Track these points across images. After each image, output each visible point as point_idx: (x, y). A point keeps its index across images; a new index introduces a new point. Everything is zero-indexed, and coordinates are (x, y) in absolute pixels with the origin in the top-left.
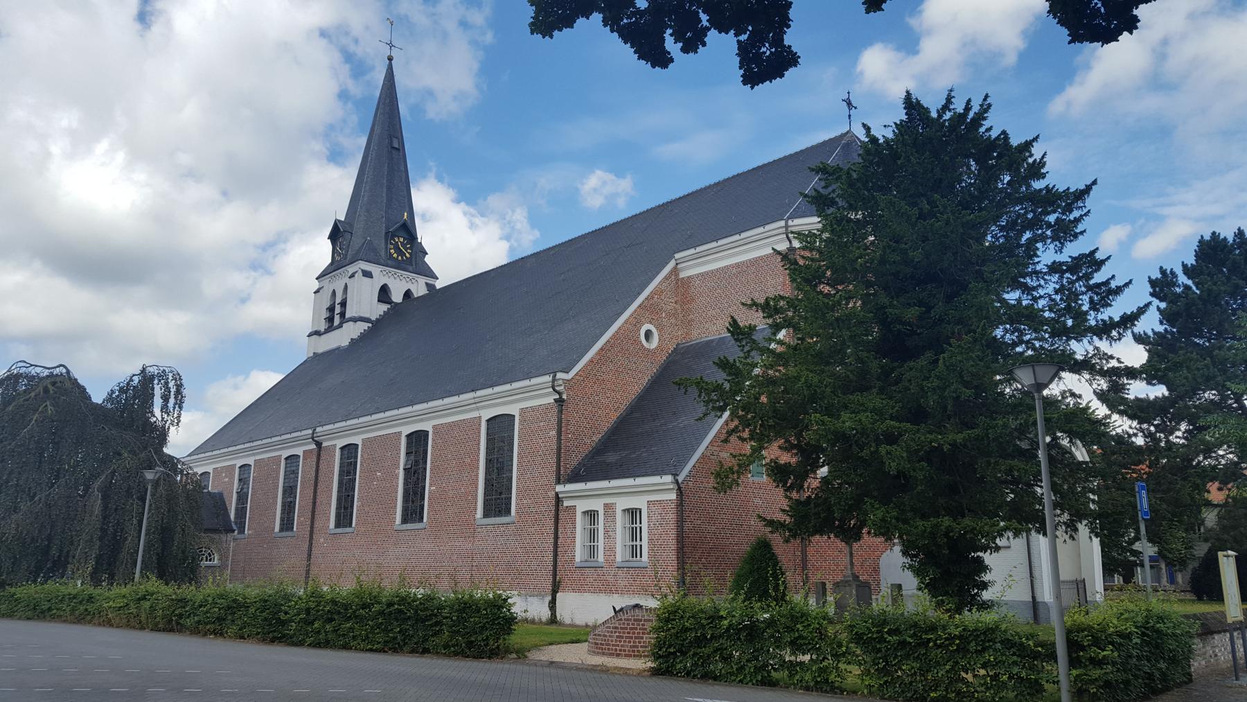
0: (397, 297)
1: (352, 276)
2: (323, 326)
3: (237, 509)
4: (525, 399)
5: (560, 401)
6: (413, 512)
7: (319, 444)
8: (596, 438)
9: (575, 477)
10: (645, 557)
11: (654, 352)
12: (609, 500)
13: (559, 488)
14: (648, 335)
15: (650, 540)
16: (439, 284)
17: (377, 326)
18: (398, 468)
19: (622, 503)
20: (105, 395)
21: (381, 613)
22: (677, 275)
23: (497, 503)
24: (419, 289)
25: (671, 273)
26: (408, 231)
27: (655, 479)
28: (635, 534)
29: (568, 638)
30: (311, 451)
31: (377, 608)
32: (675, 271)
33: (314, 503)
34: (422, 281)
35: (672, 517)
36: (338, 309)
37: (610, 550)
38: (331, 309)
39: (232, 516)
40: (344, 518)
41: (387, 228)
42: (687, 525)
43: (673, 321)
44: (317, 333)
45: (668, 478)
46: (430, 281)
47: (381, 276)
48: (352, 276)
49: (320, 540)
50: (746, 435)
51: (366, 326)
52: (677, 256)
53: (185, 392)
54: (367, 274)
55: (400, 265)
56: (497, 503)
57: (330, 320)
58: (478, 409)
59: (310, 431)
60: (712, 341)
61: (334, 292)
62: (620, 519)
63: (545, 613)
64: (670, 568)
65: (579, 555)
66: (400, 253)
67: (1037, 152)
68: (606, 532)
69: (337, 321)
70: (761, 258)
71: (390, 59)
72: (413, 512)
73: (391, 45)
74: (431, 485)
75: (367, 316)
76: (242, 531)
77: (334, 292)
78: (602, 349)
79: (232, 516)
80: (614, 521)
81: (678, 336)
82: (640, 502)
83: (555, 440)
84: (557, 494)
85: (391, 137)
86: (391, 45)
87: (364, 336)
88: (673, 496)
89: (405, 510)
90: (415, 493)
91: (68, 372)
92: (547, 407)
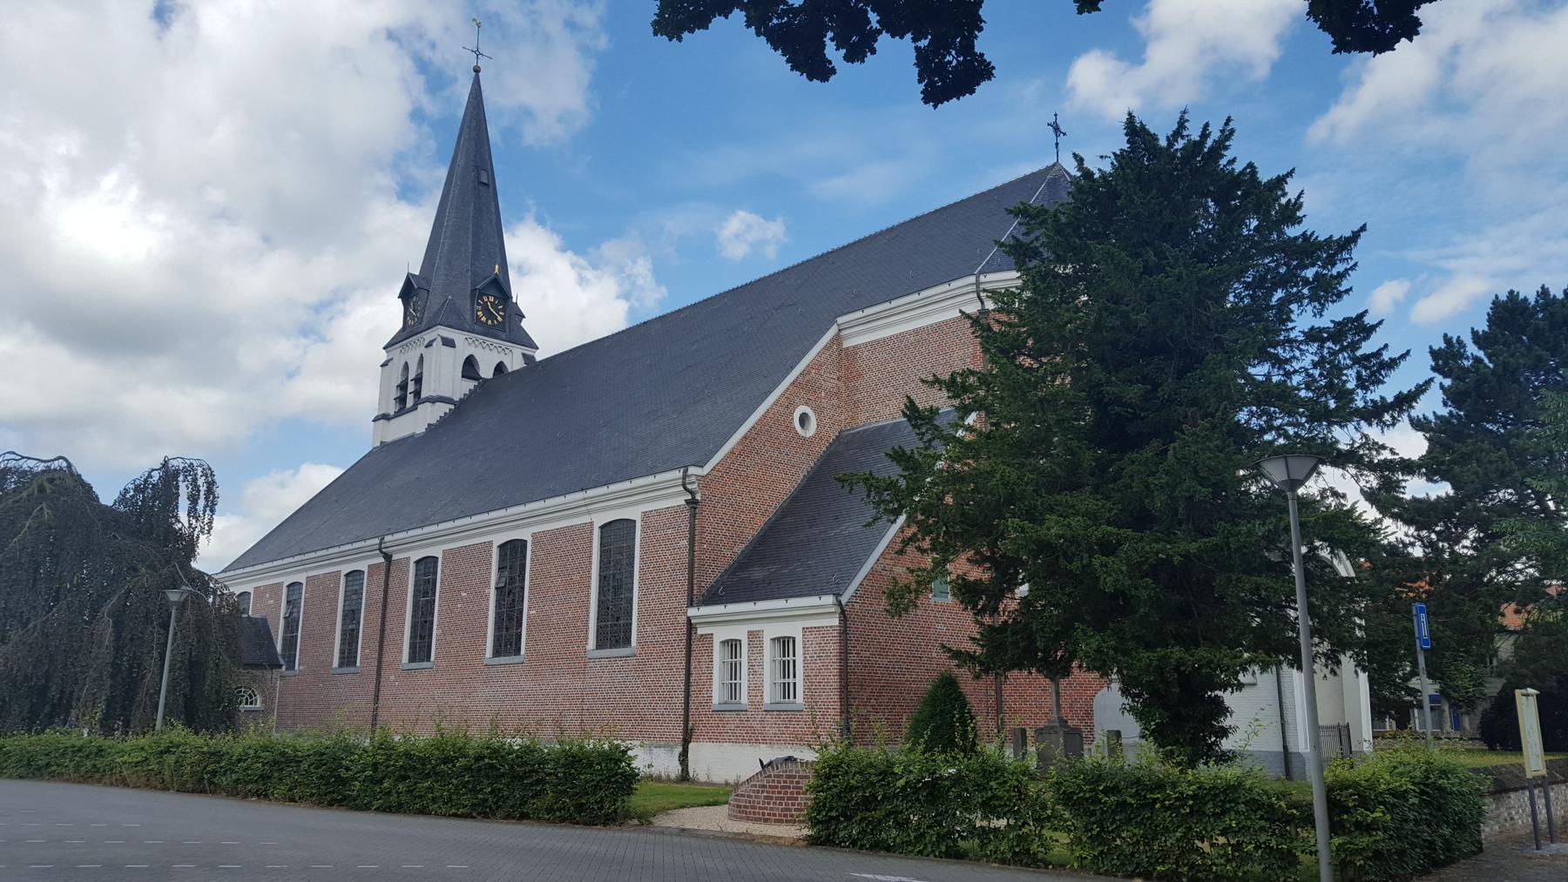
0: (486, 371)
1: (429, 345)
2: (392, 408)
3: (284, 639)
4: (648, 500)
5: (692, 503)
6: (507, 643)
7: (388, 557)
8: (739, 549)
9: (712, 598)
10: (800, 698)
11: (811, 440)
12: (754, 627)
13: (692, 612)
14: (804, 419)
15: (807, 676)
16: (539, 356)
17: (461, 408)
18: (488, 586)
19: (771, 631)
20: (116, 496)
21: (468, 769)
22: (840, 344)
23: (614, 631)
24: (514, 362)
25: (832, 341)
28: (787, 669)
29: (703, 800)
30: (378, 565)
31: (462, 762)
32: (838, 339)
33: (383, 631)
34: (518, 351)
35: (833, 647)
36: (411, 387)
37: (756, 689)
38: (403, 387)
39: (279, 648)
40: (420, 650)
41: (474, 284)
42: (853, 658)
43: (835, 401)
44: (385, 417)
45: (829, 600)
46: (528, 351)
47: (466, 343)
48: (429, 345)
49: (390, 677)
51: (445, 408)
52: (840, 320)
53: (218, 491)
54: (448, 343)
56: (614, 631)
57: (402, 400)
58: (589, 512)
60: (883, 427)
61: (406, 366)
62: (769, 652)
63: (674, 769)
65: (717, 695)
66: (491, 316)
67: (1292, 190)
68: (751, 666)
69: (410, 401)
70: (945, 323)
71: (477, 70)
72: (507, 643)
73: (478, 53)
74: (530, 608)
75: (448, 395)
76: (291, 666)
77: (406, 366)
78: (745, 437)
79: (279, 648)
80: (761, 653)
81: (842, 420)
82: (793, 629)
83: (686, 552)
84: (689, 619)
85: (478, 169)
86: (478, 53)
87: (444, 420)
89: (497, 639)
90: (510, 619)
92: (675, 511)
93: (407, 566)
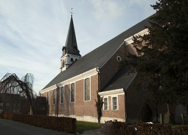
0: (74, 60)
7: (58, 87)
10: (118, 109)
12: (109, 96)
14: (119, 58)
19: (113, 96)
22: (125, 45)
25: (123, 44)
26: (76, 47)
27: (119, 90)
28: (115, 103)
34: (79, 57)
36: (64, 63)
37: (110, 107)
38: (63, 63)
45: (122, 89)
46: (80, 57)
50: (176, 19)
55: (74, 54)
59: (56, 85)
63: (97, 121)
64: (122, 103)
66: (75, 52)
71: (72, 15)
73: (72, 13)
78: (108, 62)
82: (116, 96)
85: (72, 30)
86: (72, 13)
88: (124, 94)
91: (15, 75)
92: (96, 75)
93: (70, 85)
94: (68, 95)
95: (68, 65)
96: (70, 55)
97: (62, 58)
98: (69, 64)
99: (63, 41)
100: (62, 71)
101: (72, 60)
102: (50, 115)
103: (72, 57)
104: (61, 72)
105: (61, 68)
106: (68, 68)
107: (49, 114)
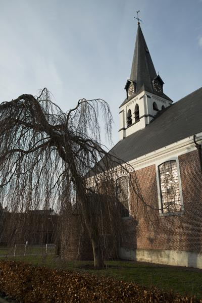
59: (192, 137)
71: (139, 24)
94: (61, 200)
95: (149, 115)
96: (151, 95)
97: (124, 108)
98: (151, 114)
99: (126, 70)
100: (127, 135)
101: (155, 106)
102: (143, 256)
103: (154, 100)
104: (124, 138)
105: (124, 129)
106: (151, 122)
107: (135, 248)
